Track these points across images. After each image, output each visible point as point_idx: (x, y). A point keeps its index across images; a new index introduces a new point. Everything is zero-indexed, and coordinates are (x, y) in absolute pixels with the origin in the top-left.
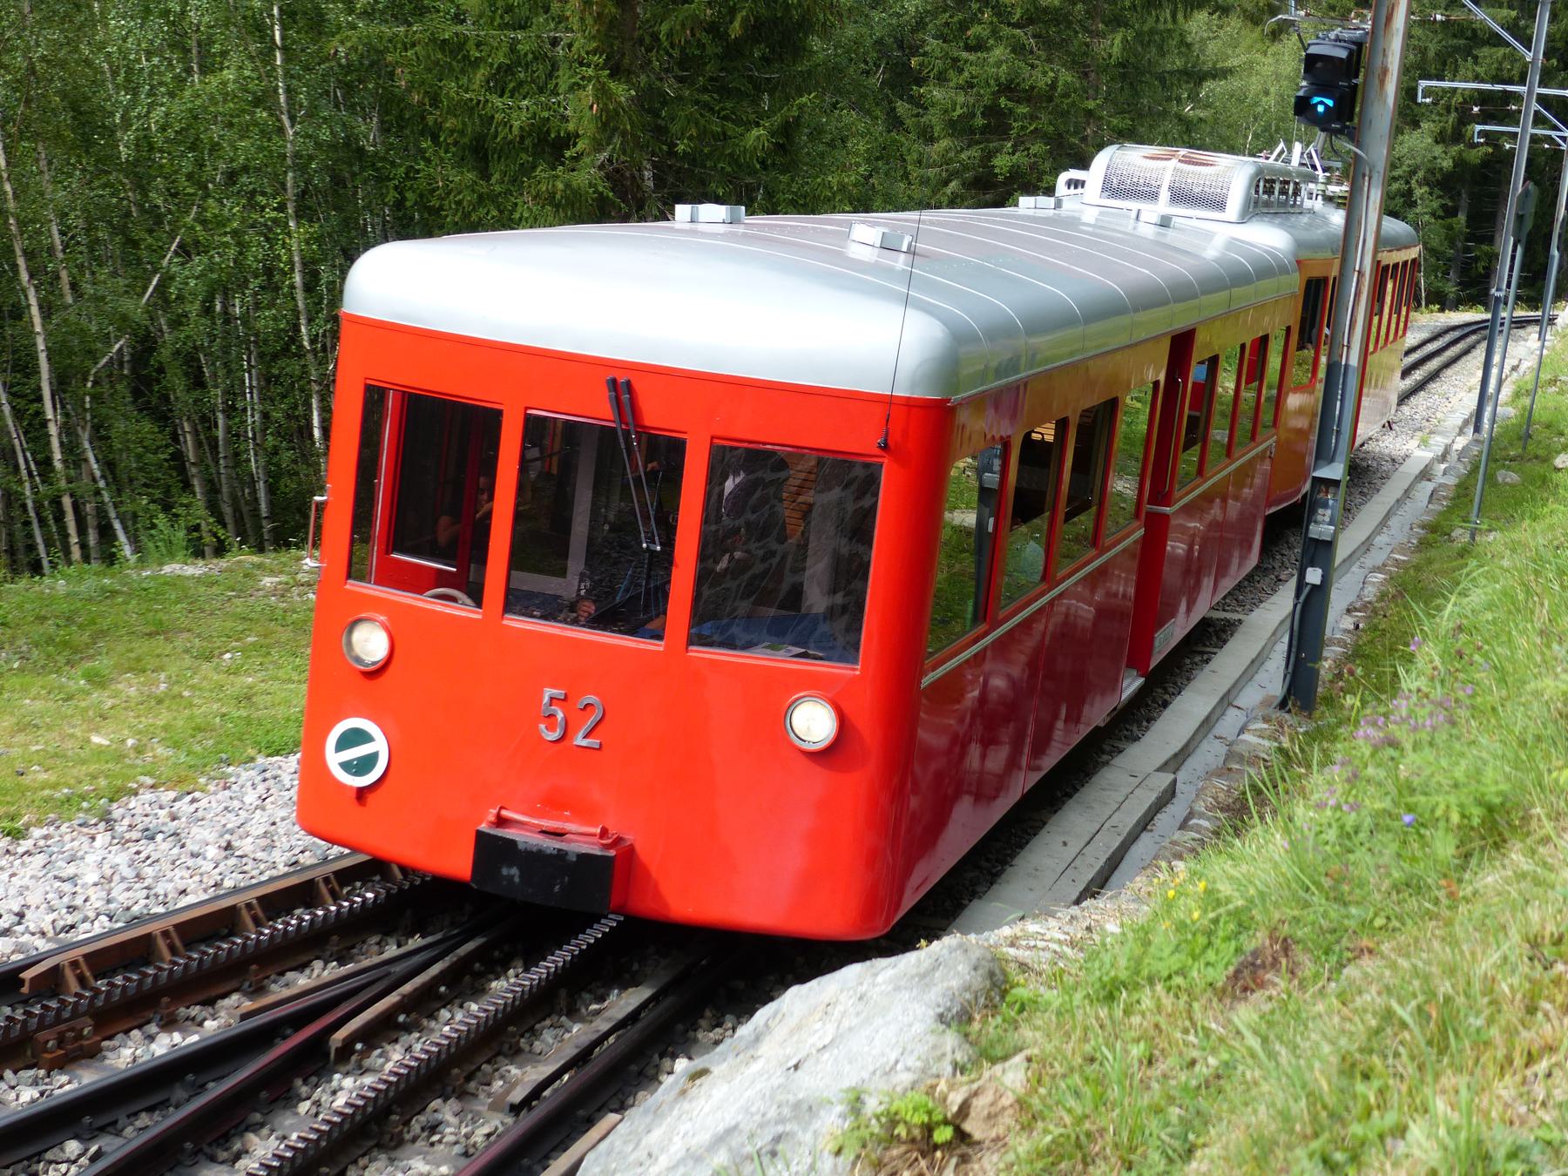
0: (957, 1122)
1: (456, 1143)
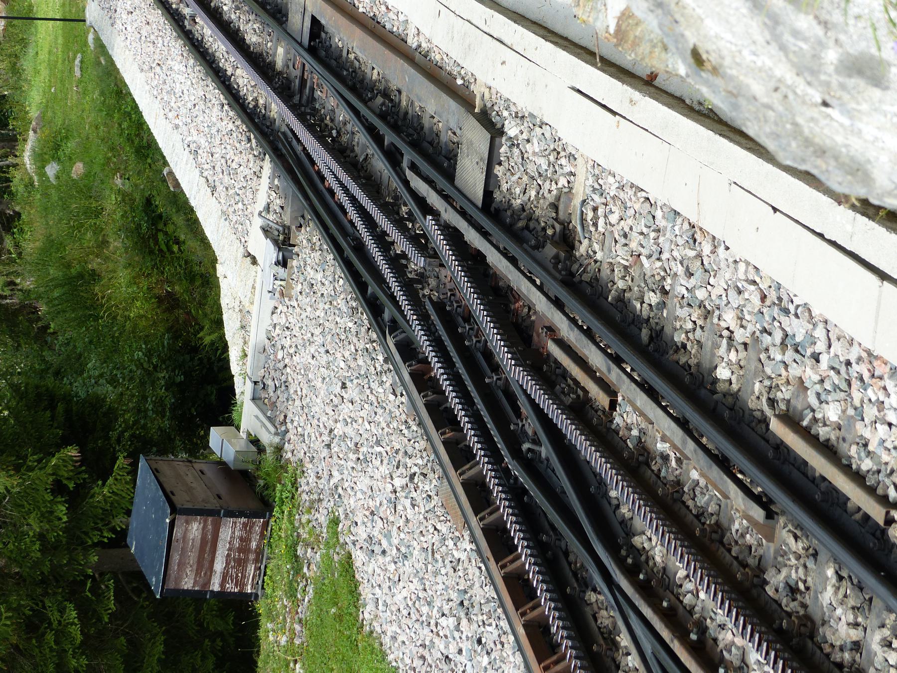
1: (805, 566)
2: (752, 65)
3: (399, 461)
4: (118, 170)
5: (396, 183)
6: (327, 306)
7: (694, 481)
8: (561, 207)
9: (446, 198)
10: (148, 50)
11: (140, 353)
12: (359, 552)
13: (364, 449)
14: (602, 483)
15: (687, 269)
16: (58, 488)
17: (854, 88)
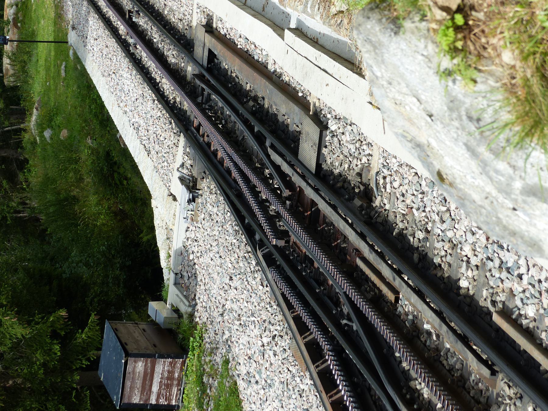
0: (452, 13)
1: (515, 404)
2: (472, 184)
3: (266, 327)
4: (89, 134)
5: (262, 155)
6: (220, 229)
7: (447, 348)
8: (364, 175)
9: (292, 166)
10: (107, 63)
11: (104, 247)
12: (241, 382)
13: (243, 318)
14: (390, 348)
15: (441, 218)
16: (54, 335)
17: (531, 202)
